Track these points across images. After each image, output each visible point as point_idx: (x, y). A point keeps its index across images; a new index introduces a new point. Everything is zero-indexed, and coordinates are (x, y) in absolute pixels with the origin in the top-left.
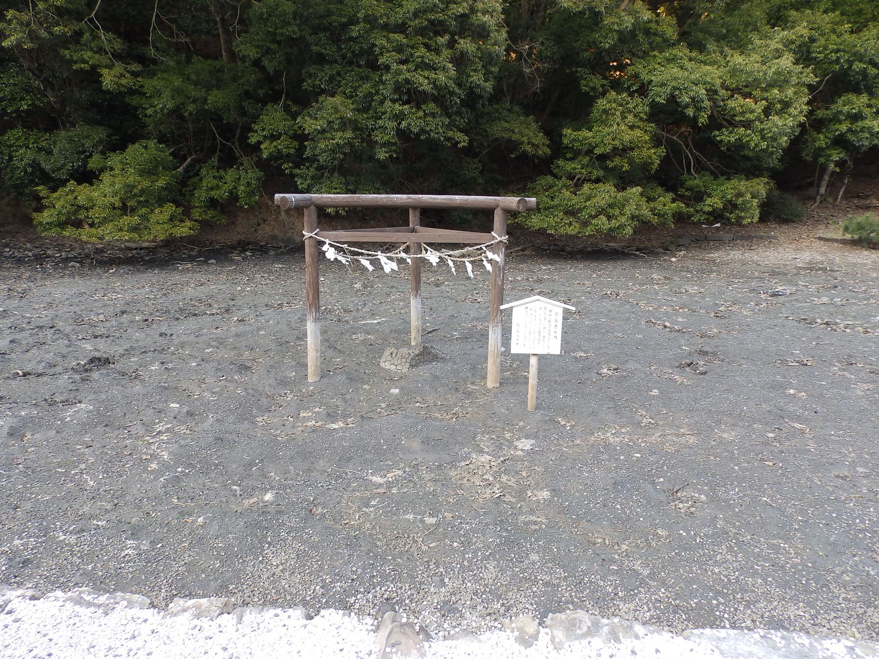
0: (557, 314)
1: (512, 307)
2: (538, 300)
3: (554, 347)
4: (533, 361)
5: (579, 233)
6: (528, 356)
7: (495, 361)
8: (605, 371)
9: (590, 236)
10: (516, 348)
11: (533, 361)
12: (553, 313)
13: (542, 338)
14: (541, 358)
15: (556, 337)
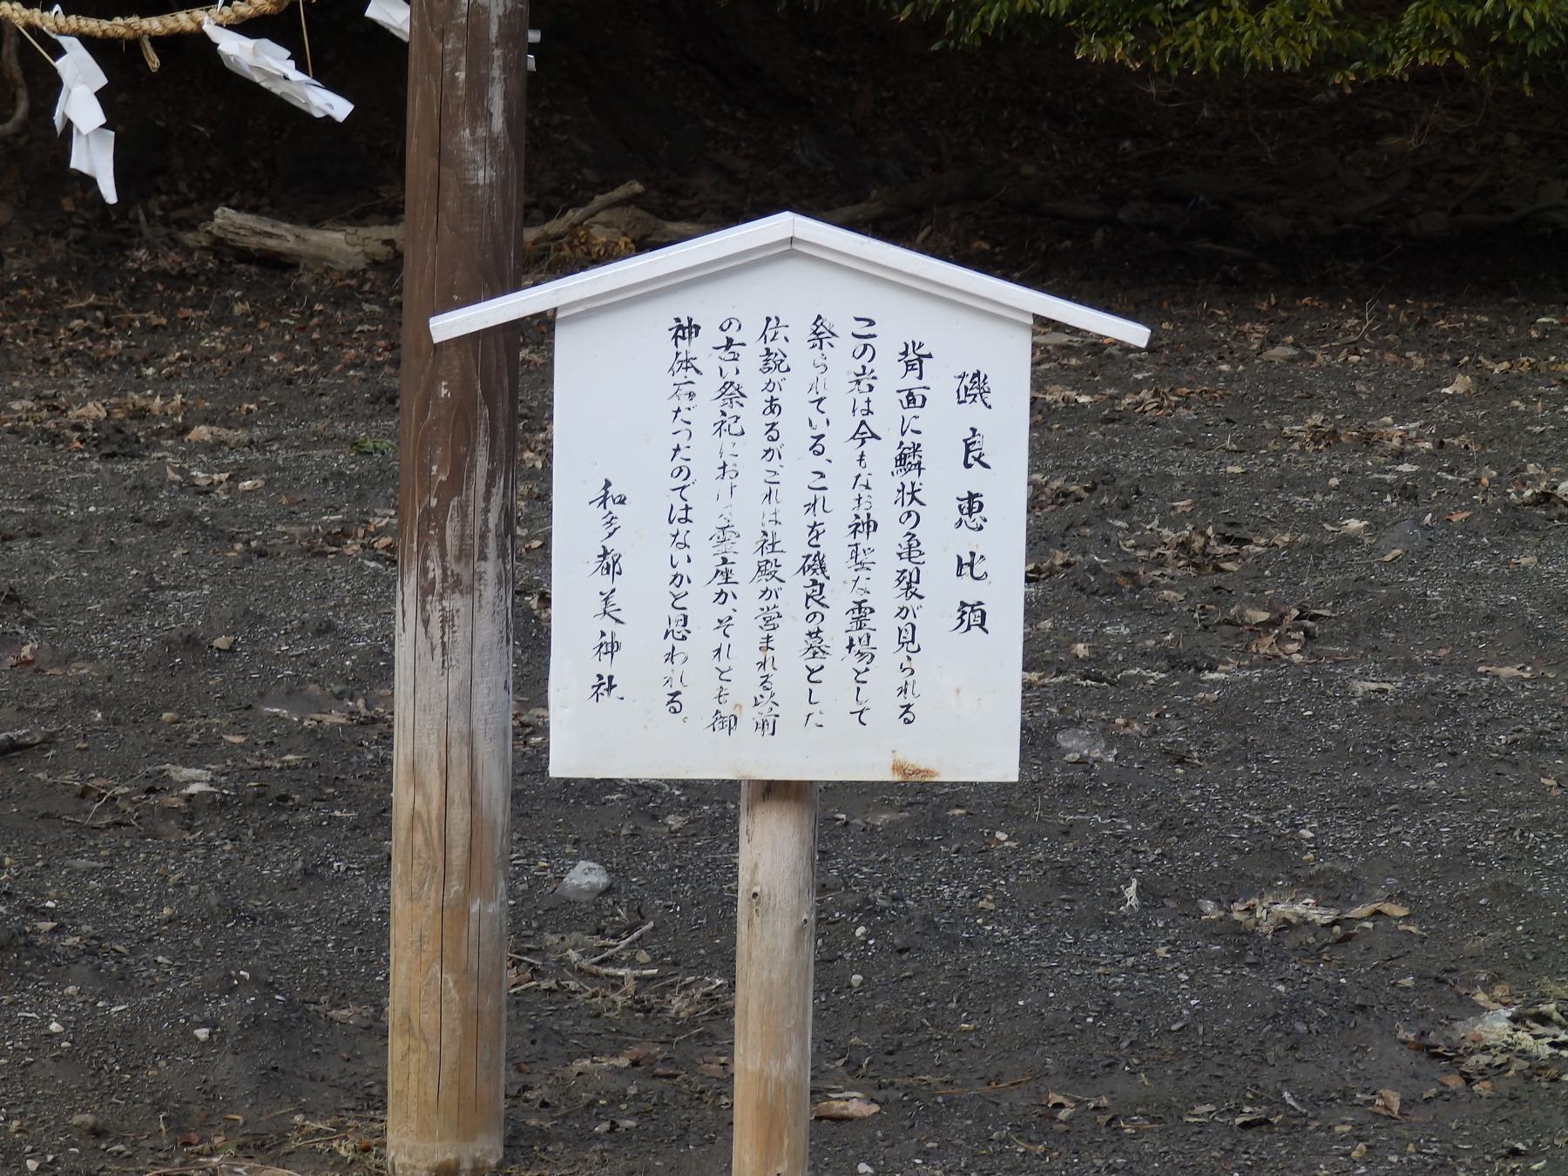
0: (975, 387)
1: (541, 328)
2: (790, 250)
3: (965, 719)
4: (770, 855)
5: (1330, 59)
6: (711, 809)
7: (452, 914)
8: (1496, 1026)
9: (1424, 78)
10: (588, 740)
11: (770, 855)
12: (940, 380)
13: (837, 626)
14: (829, 809)
15: (973, 616)
